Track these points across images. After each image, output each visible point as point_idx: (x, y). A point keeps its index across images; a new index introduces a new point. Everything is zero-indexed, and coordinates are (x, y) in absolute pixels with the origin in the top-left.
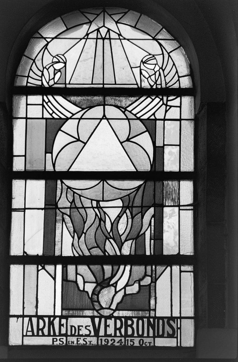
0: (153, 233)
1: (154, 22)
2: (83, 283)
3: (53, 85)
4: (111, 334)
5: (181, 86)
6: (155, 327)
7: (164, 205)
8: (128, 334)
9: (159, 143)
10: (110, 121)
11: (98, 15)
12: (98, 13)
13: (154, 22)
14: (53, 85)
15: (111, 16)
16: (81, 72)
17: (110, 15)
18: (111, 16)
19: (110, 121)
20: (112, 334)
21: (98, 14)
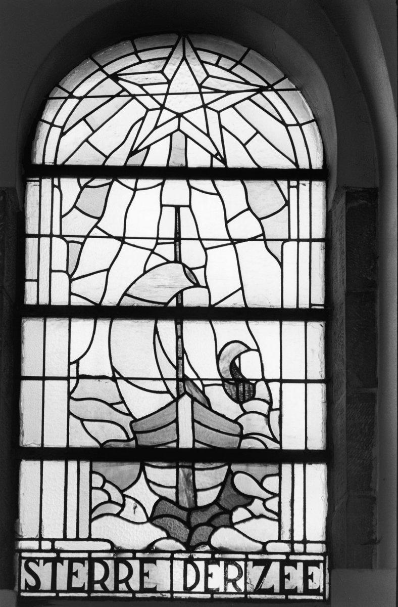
0: (114, 555)
1: (377, 409)
2: (67, 364)
3: (105, 162)
4: (272, 586)
5: (45, 161)
6: (105, 597)
7: (327, 557)
8: (286, 588)
9: (158, 561)
10: (166, 381)
11: (174, 48)
12: (173, 44)
13: (377, 409)
14: (105, 162)
15: (198, 51)
16: (111, 141)
17: (195, 50)
18: (198, 51)
19: (166, 381)
20: (275, 587)
21: (173, 46)
